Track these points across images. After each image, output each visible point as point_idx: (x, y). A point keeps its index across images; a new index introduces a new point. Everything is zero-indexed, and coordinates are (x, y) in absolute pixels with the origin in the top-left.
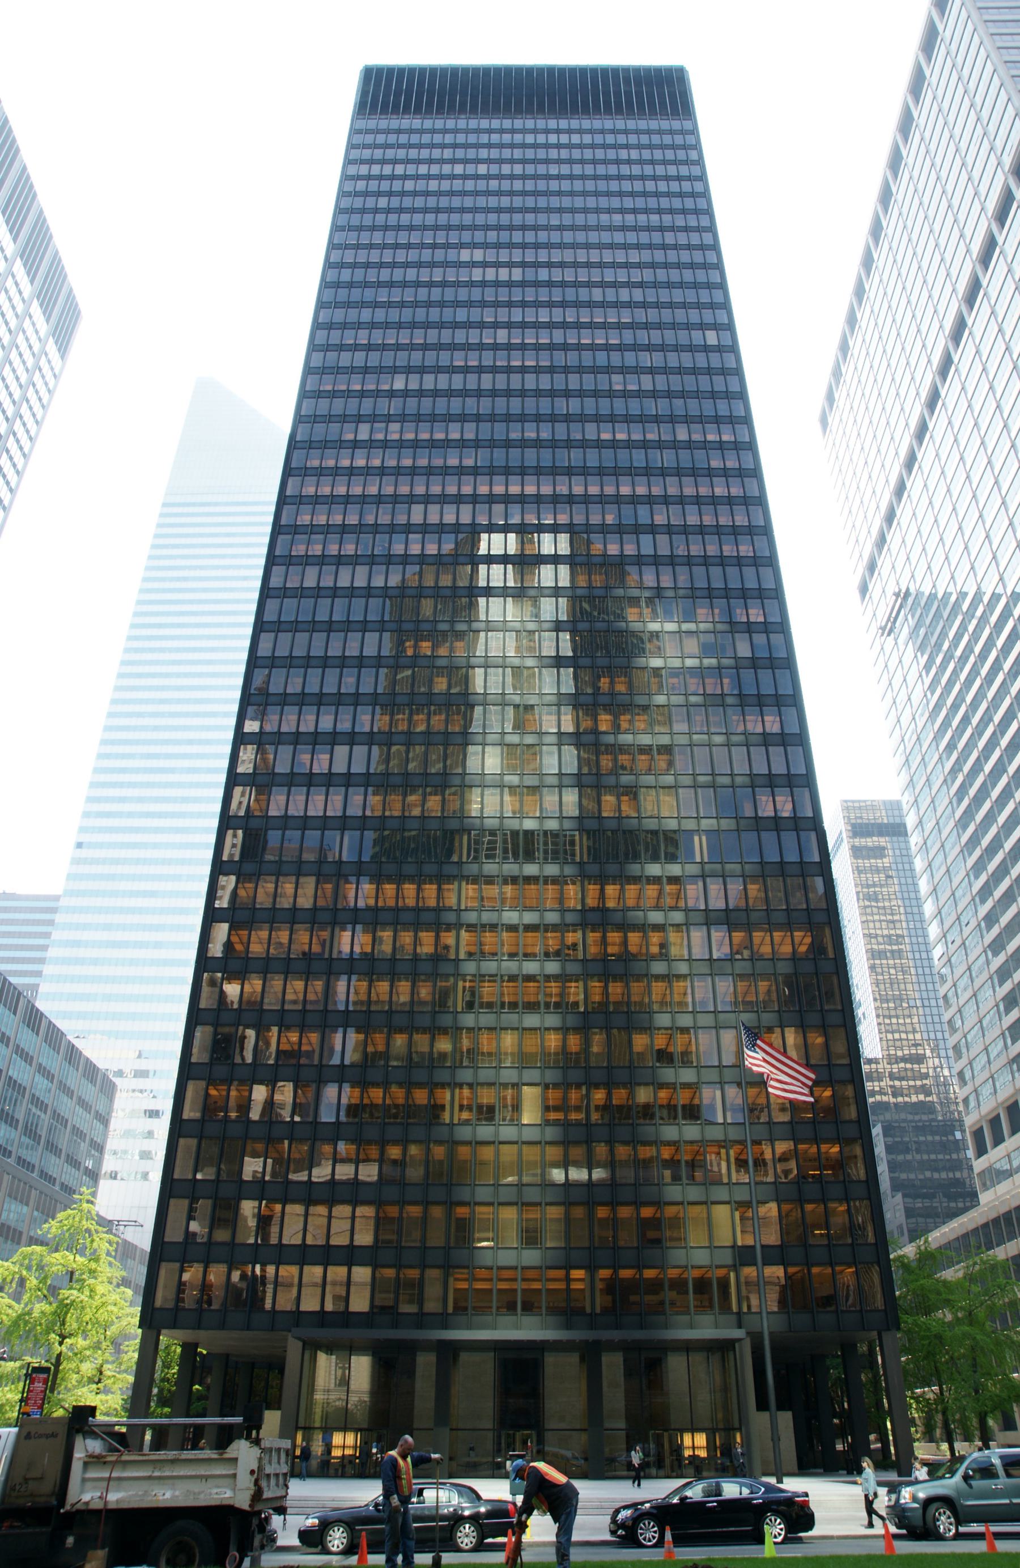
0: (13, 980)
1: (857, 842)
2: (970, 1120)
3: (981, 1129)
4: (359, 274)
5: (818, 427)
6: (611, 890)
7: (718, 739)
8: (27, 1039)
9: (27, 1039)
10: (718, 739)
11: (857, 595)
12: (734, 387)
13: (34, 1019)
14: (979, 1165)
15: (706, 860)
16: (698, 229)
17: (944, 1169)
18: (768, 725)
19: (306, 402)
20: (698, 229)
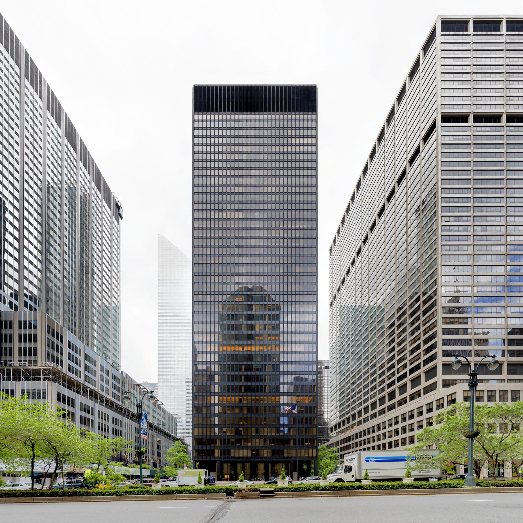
11: (329, 306)
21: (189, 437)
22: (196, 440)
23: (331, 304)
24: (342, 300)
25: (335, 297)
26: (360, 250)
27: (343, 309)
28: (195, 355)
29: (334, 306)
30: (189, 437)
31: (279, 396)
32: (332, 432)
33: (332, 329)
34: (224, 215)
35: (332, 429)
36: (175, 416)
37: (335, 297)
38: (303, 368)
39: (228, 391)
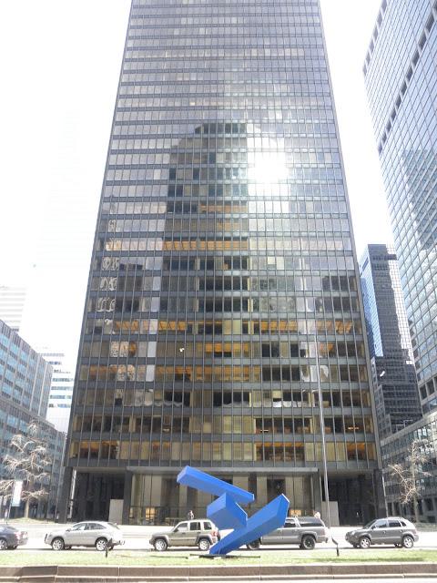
0: (8, 324)
1: (375, 262)
2: (420, 384)
3: (424, 386)
4: (296, 10)
5: (362, 73)
6: (270, 243)
7: (312, 150)
8: (14, 349)
9: (14, 349)
10: (312, 150)
11: (377, 152)
12: (319, 43)
13: (17, 341)
14: (423, 402)
15: (306, 289)
16: (312, 15)
17: (403, 394)
18: (337, 246)
19: (126, 64)
20: (312, 15)
21: (66, 406)
22: (79, 418)
23: (380, 149)
24: (402, 139)
25: (385, 139)
26: (424, 39)
27: (407, 156)
28: (102, 237)
29: (385, 151)
30: (66, 406)
31: (161, 332)
32: (424, 396)
33: (390, 197)
34: (215, 31)
35: (423, 389)
36: (48, 359)
37: (385, 139)
38: (135, 245)
39: (328, 308)
